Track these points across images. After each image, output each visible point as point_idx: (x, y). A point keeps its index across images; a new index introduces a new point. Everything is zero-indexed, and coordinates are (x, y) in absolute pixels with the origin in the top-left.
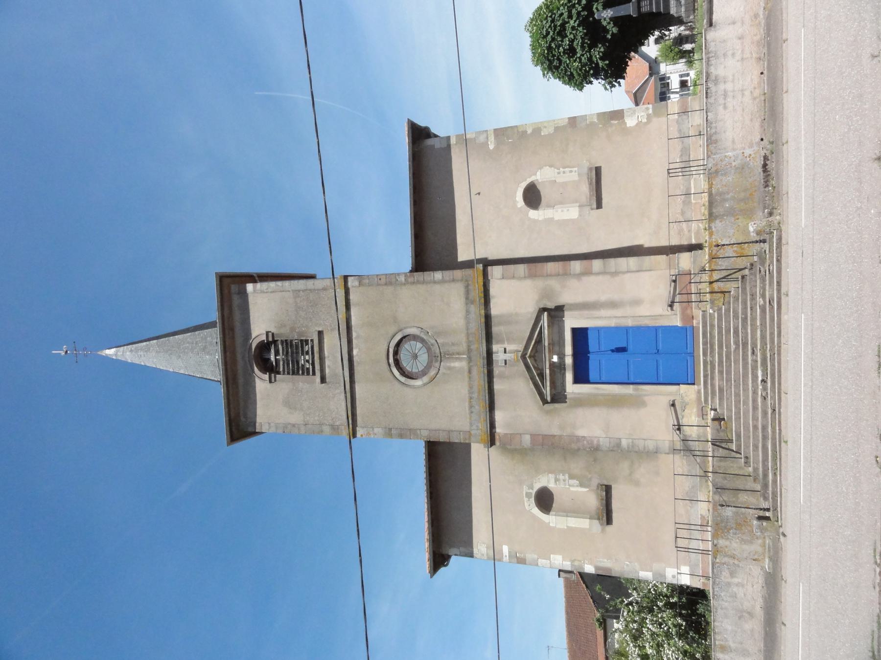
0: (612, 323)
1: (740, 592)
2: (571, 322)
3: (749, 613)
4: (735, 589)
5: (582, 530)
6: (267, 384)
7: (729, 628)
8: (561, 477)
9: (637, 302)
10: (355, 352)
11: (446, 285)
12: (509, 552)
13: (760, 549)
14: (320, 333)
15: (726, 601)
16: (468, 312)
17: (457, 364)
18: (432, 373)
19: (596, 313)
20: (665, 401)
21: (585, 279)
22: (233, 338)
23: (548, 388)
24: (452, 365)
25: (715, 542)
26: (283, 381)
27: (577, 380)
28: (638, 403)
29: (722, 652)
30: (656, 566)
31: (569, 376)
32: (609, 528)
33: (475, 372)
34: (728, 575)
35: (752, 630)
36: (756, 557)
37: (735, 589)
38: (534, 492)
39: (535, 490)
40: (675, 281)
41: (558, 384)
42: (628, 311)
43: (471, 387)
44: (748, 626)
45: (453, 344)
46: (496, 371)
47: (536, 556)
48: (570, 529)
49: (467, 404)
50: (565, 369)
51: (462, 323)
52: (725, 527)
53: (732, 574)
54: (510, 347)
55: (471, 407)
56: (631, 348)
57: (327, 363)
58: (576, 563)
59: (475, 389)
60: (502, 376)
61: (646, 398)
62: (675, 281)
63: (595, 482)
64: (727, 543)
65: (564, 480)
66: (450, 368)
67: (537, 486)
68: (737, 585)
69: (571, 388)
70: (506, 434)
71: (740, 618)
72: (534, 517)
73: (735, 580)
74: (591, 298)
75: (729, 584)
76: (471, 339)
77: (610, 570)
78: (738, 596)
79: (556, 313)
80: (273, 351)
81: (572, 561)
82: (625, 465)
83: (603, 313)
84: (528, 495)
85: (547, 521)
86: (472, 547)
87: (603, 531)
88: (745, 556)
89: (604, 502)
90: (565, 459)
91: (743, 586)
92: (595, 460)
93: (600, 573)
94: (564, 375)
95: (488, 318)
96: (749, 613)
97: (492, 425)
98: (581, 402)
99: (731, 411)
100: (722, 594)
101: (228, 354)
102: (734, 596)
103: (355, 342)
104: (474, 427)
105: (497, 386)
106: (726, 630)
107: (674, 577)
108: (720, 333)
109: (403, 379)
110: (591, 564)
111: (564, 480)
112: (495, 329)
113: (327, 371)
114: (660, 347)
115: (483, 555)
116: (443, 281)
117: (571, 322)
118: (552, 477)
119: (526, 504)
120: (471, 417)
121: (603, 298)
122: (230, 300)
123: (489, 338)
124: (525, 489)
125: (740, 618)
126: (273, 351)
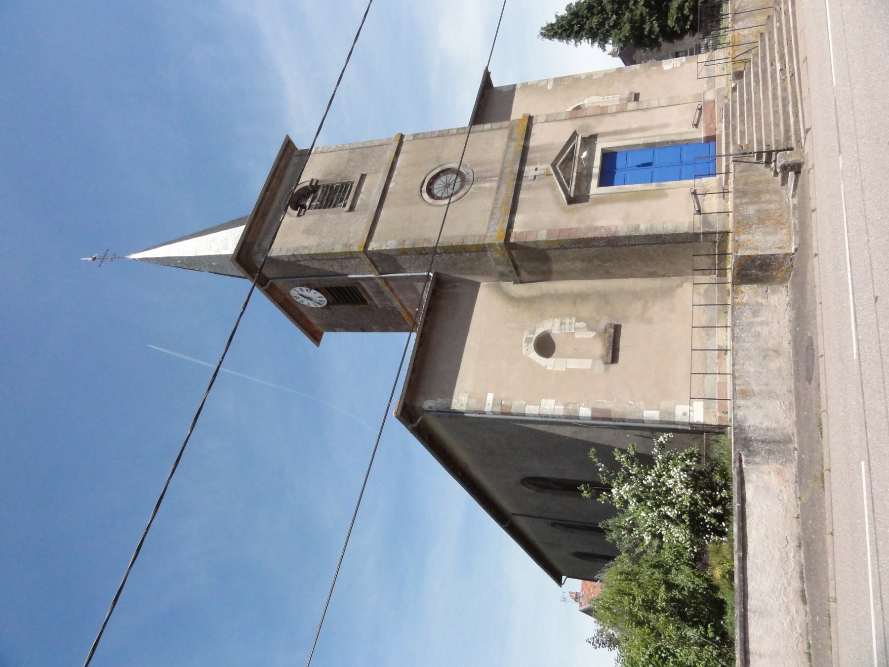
0: (641, 141)
1: (764, 331)
2: (601, 145)
3: (775, 351)
4: (759, 329)
5: (582, 372)
6: (296, 219)
7: (752, 369)
8: (568, 320)
9: (666, 126)
10: (391, 185)
11: (493, 132)
12: (494, 400)
13: (785, 238)
14: (363, 177)
15: (748, 342)
16: (508, 147)
17: (487, 185)
18: (461, 193)
19: (628, 136)
20: (687, 191)
21: (619, 115)
22: (279, 185)
23: (573, 187)
24: (483, 185)
25: (737, 238)
26: (310, 214)
27: (601, 184)
28: (660, 194)
29: (743, 398)
30: (664, 404)
31: (594, 182)
32: (614, 367)
33: (503, 189)
34: (750, 315)
35: (779, 370)
36: (781, 245)
37: (759, 329)
38: (534, 337)
39: (536, 335)
40: (700, 109)
41: (583, 188)
42: (657, 132)
43: (496, 200)
44: (774, 365)
45: (488, 171)
46: (524, 184)
47: (524, 402)
48: (569, 371)
49: (489, 214)
50: (591, 177)
51: (500, 155)
52: (747, 224)
53: (755, 313)
54: (539, 167)
55: (492, 214)
56: (656, 162)
57: (361, 196)
58: (571, 407)
59: (501, 201)
60: (529, 188)
61: (668, 191)
62: (700, 109)
63: (604, 322)
64: (750, 237)
65: (570, 324)
66: (479, 188)
67: (539, 331)
68: (761, 323)
69: (594, 188)
70: (522, 232)
71: (764, 357)
72: (531, 362)
73: (759, 319)
74: (624, 127)
75: (751, 324)
76: (506, 165)
77: (609, 411)
78: (763, 335)
79: (590, 141)
80: (310, 199)
81: (566, 405)
82: (638, 306)
83: (633, 135)
84: (528, 340)
85: (544, 365)
86: (452, 398)
87: (606, 370)
88: (769, 246)
89: (612, 338)
90: (574, 303)
91: (767, 324)
92: (606, 303)
93: (597, 415)
94: (589, 182)
95: (525, 150)
96: (775, 351)
97: (510, 226)
98: (601, 200)
99: (752, 136)
100: (743, 336)
101: (274, 180)
102: (758, 335)
103: (394, 178)
104: (492, 230)
105: (522, 196)
106: (748, 372)
107: (685, 414)
108: (742, 104)
109: (430, 201)
110: (587, 406)
111: (570, 324)
112: (530, 156)
113: (359, 202)
114: (684, 159)
115: (462, 405)
116: (492, 129)
117: (601, 145)
118: (557, 321)
119: (524, 349)
120: (490, 222)
121: (634, 126)
122: (290, 159)
123: (523, 161)
124: (526, 334)
125: (764, 357)
126: (310, 199)
